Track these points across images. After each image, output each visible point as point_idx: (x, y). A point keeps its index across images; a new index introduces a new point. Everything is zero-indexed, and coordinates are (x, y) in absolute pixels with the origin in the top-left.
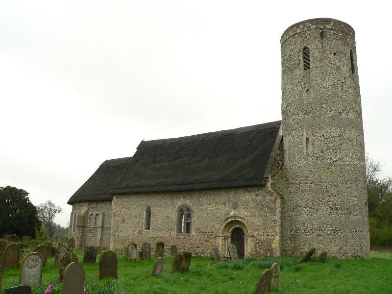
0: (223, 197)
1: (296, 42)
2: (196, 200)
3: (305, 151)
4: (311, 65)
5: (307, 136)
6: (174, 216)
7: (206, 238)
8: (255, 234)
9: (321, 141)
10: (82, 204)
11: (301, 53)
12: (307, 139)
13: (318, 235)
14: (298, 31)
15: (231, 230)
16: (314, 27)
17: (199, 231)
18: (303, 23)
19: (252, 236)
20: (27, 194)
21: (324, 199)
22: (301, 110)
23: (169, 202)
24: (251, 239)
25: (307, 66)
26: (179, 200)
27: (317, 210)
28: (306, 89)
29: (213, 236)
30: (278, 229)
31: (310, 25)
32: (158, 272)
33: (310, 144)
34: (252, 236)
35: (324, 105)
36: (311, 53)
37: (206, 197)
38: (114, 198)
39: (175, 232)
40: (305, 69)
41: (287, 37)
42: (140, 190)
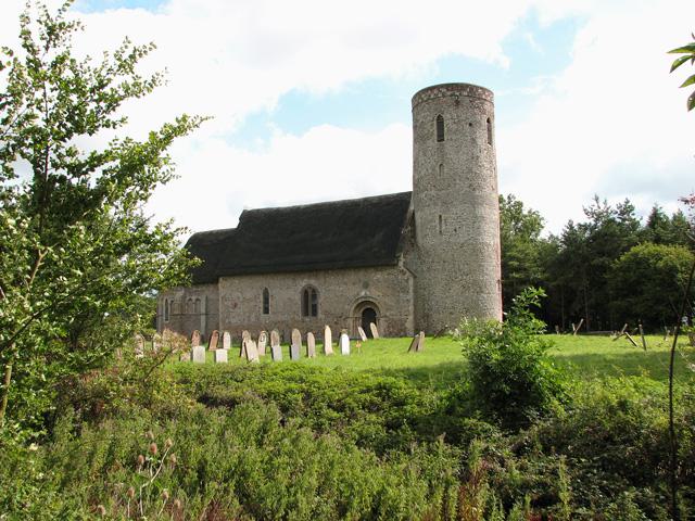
0: (352, 276)
2: (322, 280)
6: (298, 298)
11: (435, 122)
12: (440, 217)
13: (451, 313)
16: (449, 93)
19: (386, 316)
25: (441, 138)
30: (411, 308)
38: (221, 279)
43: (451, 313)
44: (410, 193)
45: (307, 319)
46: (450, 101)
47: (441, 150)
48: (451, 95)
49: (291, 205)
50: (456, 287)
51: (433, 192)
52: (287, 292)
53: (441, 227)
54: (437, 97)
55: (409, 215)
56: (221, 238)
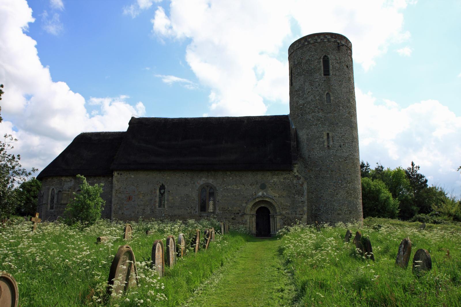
0: (250, 177)
1: (316, 50)
3: (326, 144)
4: (331, 72)
5: (328, 132)
6: (195, 195)
7: (233, 216)
8: (284, 212)
9: (339, 137)
11: (322, 60)
12: (328, 134)
13: (339, 214)
14: (319, 41)
15: (256, 209)
16: (333, 40)
19: (281, 214)
21: (342, 185)
22: (322, 110)
24: (279, 217)
25: (327, 73)
27: (337, 194)
28: (327, 92)
29: (240, 214)
30: (305, 209)
31: (330, 37)
33: (331, 139)
34: (281, 214)
35: (341, 108)
36: (330, 62)
37: (231, 178)
38: (115, 174)
40: (325, 75)
43: (339, 214)
44: (286, 117)
48: (335, 42)
51: (320, 114)
52: (185, 187)
53: (328, 143)
55: (292, 132)
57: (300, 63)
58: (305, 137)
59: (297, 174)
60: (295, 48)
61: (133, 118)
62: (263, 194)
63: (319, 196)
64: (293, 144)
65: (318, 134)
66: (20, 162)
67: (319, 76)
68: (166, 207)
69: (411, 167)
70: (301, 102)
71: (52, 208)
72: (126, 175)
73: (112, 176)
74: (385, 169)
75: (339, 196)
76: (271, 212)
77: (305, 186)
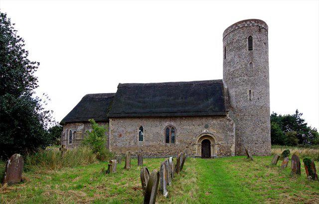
0: (197, 121)
1: (243, 32)
2: (178, 123)
4: (254, 48)
6: (162, 133)
8: (220, 143)
10: (77, 124)
11: (247, 40)
13: (256, 143)
16: (256, 24)
17: (181, 141)
18: (250, 20)
20: (120, 84)
23: (158, 123)
25: (250, 48)
26: (166, 122)
30: (234, 140)
32: (128, 167)
33: (252, 94)
36: (253, 40)
38: (111, 120)
39: (164, 142)
41: (237, 28)
42: (135, 115)
45: (168, 145)
46: (256, 29)
47: (251, 55)
49: (270, 83)
50: (259, 130)
51: (246, 78)
54: (249, 26)
55: (225, 91)
56: (106, 97)
57: (231, 43)
58: (234, 93)
59: (229, 118)
60: (228, 32)
61: (120, 84)
62: (206, 131)
63: (243, 132)
64: (226, 98)
65: (243, 92)
66: (52, 115)
67: (246, 51)
68: (144, 140)
69: (295, 113)
70: (232, 70)
71: (70, 142)
72: (117, 121)
73: (108, 122)
74: (291, 115)
75: (256, 132)
76: (212, 143)
77: (234, 126)
